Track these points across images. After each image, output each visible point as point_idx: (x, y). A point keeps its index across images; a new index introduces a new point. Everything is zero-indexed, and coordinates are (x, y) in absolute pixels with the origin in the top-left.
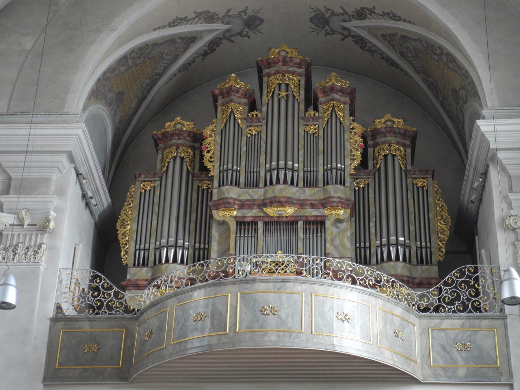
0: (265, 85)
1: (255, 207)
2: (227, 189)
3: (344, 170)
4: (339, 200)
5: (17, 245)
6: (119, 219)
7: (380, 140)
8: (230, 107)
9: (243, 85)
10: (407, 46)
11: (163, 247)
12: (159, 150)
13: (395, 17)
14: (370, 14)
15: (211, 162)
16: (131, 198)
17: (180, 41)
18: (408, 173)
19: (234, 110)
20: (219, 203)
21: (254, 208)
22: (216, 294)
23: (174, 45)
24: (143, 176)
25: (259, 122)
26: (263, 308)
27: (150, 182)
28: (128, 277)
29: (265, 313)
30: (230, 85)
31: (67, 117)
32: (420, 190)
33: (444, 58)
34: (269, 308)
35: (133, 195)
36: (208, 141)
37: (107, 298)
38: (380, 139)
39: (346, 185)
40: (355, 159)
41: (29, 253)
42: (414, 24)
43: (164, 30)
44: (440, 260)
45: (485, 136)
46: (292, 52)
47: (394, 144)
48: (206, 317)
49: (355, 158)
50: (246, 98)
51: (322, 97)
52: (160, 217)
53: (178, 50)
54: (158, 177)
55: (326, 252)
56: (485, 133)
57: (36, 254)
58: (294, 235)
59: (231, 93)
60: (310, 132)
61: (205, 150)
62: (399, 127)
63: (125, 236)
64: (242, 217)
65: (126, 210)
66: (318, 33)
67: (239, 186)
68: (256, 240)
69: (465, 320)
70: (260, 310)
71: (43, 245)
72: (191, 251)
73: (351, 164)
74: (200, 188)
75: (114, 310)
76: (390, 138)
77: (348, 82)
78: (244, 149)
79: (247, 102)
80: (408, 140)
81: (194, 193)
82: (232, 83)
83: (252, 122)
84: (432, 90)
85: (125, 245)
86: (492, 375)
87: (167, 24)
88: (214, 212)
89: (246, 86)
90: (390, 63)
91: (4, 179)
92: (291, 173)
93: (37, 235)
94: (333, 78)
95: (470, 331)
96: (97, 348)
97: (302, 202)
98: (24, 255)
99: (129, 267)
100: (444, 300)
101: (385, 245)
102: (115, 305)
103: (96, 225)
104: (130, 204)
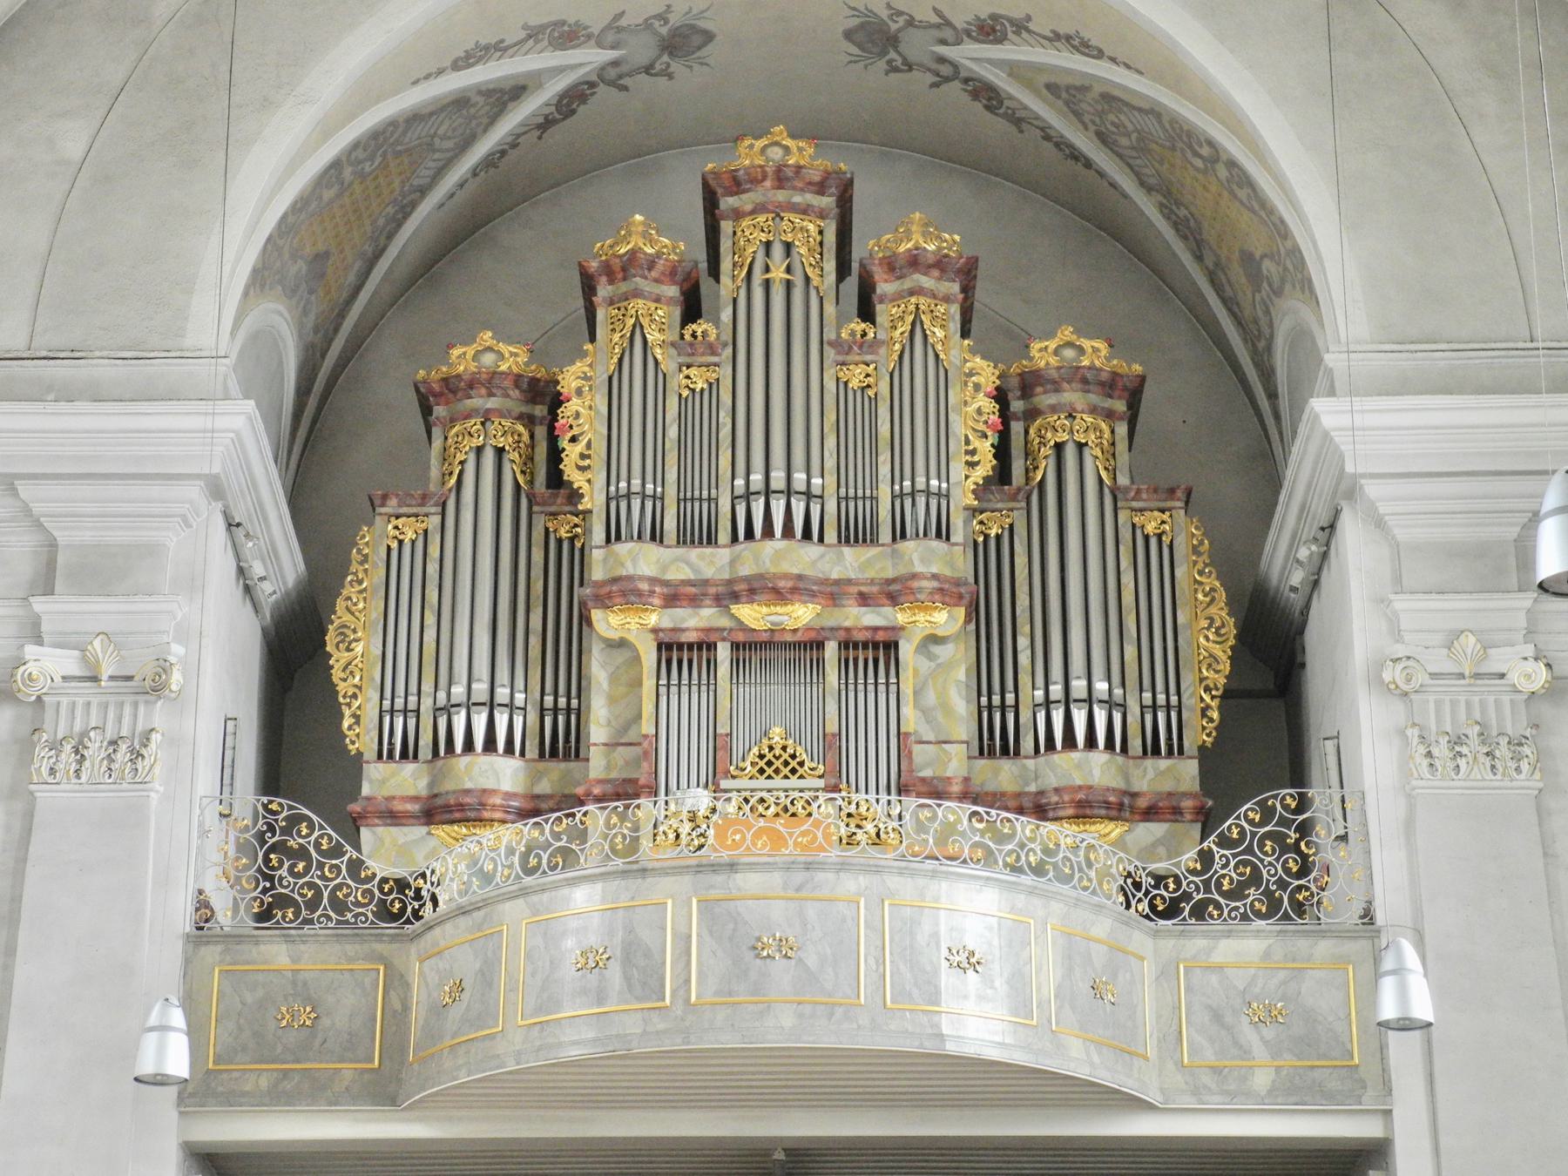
0: (725, 245)
1: (708, 602)
2: (630, 552)
3: (947, 496)
4: (935, 584)
5: (84, 734)
6: (332, 623)
7: (1044, 400)
8: (633, 312)
9: (666, 246)
10: (1117, 121)
11: (459, 705)
12: (435, 425)
13: (1084, 47)
14: (1017, 33)
15: (582, 469)
16: (362, 563)
17: (481, 100)
18: (1120, 496)
19: (645, 322)
20: (610, 592)
21: (704, 603)
22: (633, 899)
23: (464, 112)
24: (393, 502)
25: (714, 353)
26: (759, 939)
27: (413, 519)
28: (366, 790)
29: (765, 954)
30: (629, 247)
31: (195, 365)
32: (1153, 542)
33: (1222, 172)
34: (774, 940)
35: (367, 555)
36: (575, 408)
37: (332, 880)
38: (1043, 396)
39: (953, 539)
40: (977, 463)
41: (119, 756)
42: (1140, 73)
43: (441, 79)
44: (1204, 741)
45: (1332, 439)
46: (800, 150)
47: (1083, 412)
48: (608, 959)
49: (976, 458)
50: (674, 283)
51: (886, 281)
52: (446, 616)
53: (474, 123)
54: (436, 505)
55: (902, 730)
56: (1332, 434)
57: (136, 758)
58: (815, 680)
59: (633, 271)
60: (854, 384)
61: (564, 433)
62: (1097, 363)
63: (351, 673)
64: (673, 630)
65: (349, 598)
66: (866, 67)
67: (661, 541)
68: (711, 693)
69: (1271, 941)
70: (750, 945)
71: (154, 736)
72: (533, 717)
73: (967, 477)
74: (552, 536)
75: (352, 911)
76: (1072, 396)
77: (957, 238)
78: (673, 432)
79: (678, 294)
80: (1120, 398)
81: (534, 549)
82: (636, 241)
83: (693, 354)
84: (1185, 238)
85: (351, 697)
86: (1340, 1088)
87: (449, 64)
88: (596, 615)
89: (674, 248)
90: (1067, 152)
91: (36, 546)
92: (802, 505)
93: (136, 705)
94: (914, 228)
95: (1285, 971)
96: (313, 1015)
97: (835, 589)
98: (105, 762)
99: (368, 762)
100: (1219, 885)
101: (1059, 702)
102: (351, 898)
103: (265, 632)
104: (360, 582)
